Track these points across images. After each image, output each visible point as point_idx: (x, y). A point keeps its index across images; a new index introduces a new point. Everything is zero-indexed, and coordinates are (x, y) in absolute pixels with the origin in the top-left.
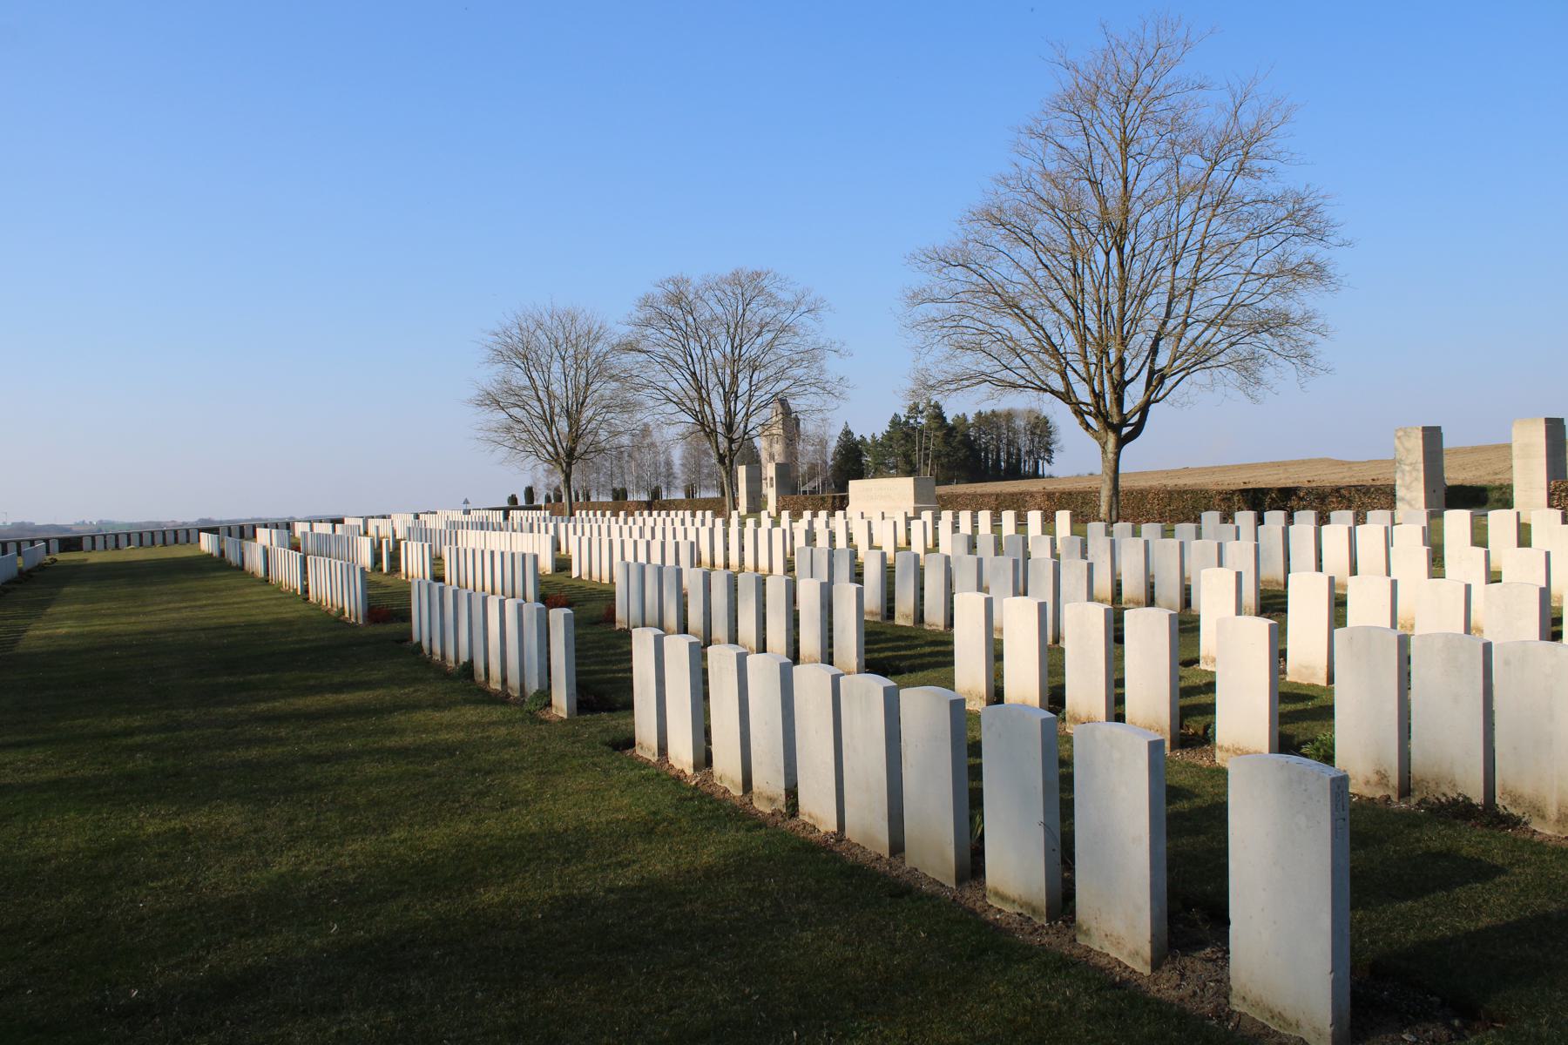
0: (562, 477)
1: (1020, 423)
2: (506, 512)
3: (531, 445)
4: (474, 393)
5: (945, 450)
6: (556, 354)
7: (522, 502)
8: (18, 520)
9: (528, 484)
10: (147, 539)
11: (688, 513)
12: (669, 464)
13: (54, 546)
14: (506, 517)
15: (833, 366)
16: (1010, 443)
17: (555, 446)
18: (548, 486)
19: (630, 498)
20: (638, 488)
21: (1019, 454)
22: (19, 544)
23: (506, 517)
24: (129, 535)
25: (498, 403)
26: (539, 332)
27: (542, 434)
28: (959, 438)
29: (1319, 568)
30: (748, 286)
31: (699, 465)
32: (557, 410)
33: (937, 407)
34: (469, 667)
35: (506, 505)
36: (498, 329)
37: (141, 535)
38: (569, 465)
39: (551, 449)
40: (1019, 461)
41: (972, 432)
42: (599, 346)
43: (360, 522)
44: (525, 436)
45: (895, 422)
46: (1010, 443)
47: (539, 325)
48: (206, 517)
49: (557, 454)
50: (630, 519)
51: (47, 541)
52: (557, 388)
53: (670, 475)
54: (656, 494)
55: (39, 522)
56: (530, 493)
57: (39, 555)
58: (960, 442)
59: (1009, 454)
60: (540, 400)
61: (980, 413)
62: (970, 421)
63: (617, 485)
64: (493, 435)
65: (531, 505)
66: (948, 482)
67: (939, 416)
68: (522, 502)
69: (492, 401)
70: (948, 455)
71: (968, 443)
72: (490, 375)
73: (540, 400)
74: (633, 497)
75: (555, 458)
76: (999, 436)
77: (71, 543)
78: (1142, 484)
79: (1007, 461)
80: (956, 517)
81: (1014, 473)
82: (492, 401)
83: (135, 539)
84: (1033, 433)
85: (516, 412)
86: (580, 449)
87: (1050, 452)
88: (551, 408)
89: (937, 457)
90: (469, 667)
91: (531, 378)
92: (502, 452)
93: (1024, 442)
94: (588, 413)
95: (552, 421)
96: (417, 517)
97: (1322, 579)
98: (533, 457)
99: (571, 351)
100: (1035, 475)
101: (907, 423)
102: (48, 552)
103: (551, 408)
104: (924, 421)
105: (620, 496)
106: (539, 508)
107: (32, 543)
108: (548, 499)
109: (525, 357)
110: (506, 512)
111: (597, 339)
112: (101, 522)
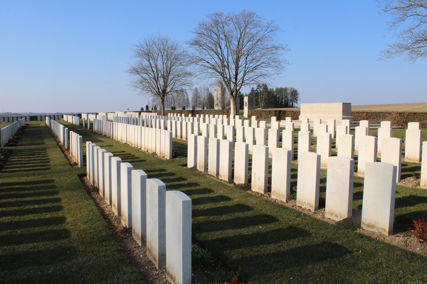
0: (161, 101)
1: (289, 91)
2: (140, 113)
3: (148, 88)
4: (129, 68)
5: (267, 98)
6: (160, 54)
7: (145, 110)
8: (7, 112)
9: (147, 104)
10: (11, 120)
11: (225, 116)
12: (188, 100)
13: (28, 119)
14: (140, 114)
15: (281, 55)
16: (286, 97)
17: (158, 88)
18: (152, 105)
19: (176, 109)
20: (179, 107)
21: (288, 101)
22: (17, 117)
23: (140, 114)
24: (4, 118)
25: (137, 72)
26: (154, 46)
27: (153, 82)
28: (271, 95)
29: (327, 131)
30: (247, 20)
31: (197, 101)
32: (160, 75)
33: (266, 86)
34: (126, 143)
35: (140, 110)
36: (138, 44)
37: (8, 118)
38: (164, 96)
39: (157, 90)
40: (288, 102)
41: (275, 94)
42: (176, 52)
43: (105, 114)
44: (147, 85)
45: (253, 90)
46: (286, 97)
47: (154, 43)
48: (58, 112)
49: (159, 92)
50: (187, 118)
51: (26, 117)
52: (160, 67)
53: (188, 103)
54: (184, 108)
55: (13, 112)
56: (147, 107)
57: (23, 122)
58: (272, 96)
59: (285, 101)
60: (153, 71)
61: (277, 88)
62: (274, 90)
63: (173, 105)
64: (136, 85)
65: (148, 111)
66: (268, 108)
67: (266, 87)
68: (145, 110)
69: (136, 71)
70: (268, 100)
71: (275, 97)
72: (135, 62)
73: (153, 71)
74: (178, 109)
75: (158, 93)
76: (282, 95)
77: (34, 118)
78: (357, 110)
79: (285, 103)
80: (204, 116)
81: (286, 106)
82: (136, 71)
83: (6, 119)
84: (292, 95)
85: (144, 75)
86: (168, 89)
87: (297, 100)
88: (158, 75)
89: (265, 100)
90: (126, 143)
91: (150, 63)
92: (139, 91)
93: (289, 97)
94: (170, 77)
95: (158, 79)
96: (107, 114)
97: (328, 135)
98: (150, 93)
99: (165, 53)
100: (292, 107)
101: (257, 90)
102: (26, 121)
103: (158, 75)
104: (262, 90)
105: (174, 108)
106: (151, 112)
107: (21, 118)
108: (152, 109)
109: (148, 55)
110: (140, 113)
111: (175, 49)
112: (30, 113)
